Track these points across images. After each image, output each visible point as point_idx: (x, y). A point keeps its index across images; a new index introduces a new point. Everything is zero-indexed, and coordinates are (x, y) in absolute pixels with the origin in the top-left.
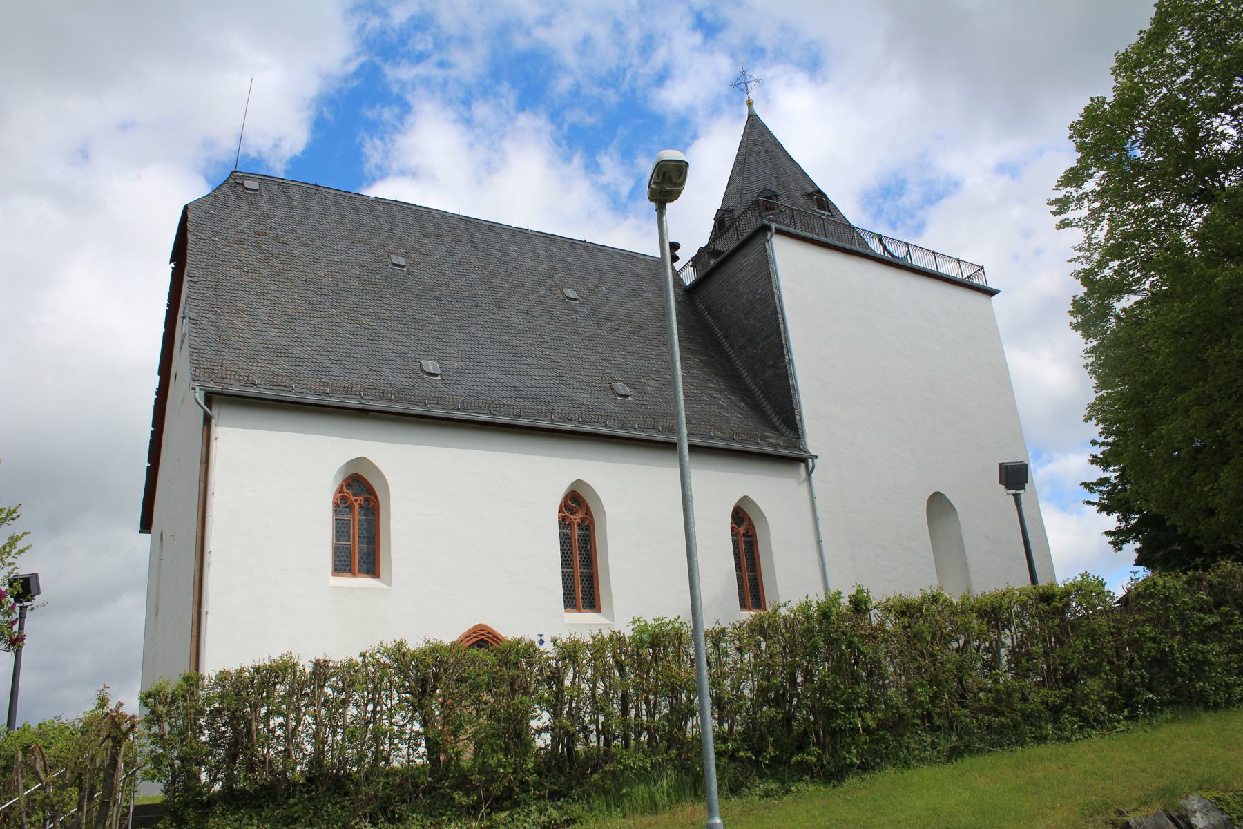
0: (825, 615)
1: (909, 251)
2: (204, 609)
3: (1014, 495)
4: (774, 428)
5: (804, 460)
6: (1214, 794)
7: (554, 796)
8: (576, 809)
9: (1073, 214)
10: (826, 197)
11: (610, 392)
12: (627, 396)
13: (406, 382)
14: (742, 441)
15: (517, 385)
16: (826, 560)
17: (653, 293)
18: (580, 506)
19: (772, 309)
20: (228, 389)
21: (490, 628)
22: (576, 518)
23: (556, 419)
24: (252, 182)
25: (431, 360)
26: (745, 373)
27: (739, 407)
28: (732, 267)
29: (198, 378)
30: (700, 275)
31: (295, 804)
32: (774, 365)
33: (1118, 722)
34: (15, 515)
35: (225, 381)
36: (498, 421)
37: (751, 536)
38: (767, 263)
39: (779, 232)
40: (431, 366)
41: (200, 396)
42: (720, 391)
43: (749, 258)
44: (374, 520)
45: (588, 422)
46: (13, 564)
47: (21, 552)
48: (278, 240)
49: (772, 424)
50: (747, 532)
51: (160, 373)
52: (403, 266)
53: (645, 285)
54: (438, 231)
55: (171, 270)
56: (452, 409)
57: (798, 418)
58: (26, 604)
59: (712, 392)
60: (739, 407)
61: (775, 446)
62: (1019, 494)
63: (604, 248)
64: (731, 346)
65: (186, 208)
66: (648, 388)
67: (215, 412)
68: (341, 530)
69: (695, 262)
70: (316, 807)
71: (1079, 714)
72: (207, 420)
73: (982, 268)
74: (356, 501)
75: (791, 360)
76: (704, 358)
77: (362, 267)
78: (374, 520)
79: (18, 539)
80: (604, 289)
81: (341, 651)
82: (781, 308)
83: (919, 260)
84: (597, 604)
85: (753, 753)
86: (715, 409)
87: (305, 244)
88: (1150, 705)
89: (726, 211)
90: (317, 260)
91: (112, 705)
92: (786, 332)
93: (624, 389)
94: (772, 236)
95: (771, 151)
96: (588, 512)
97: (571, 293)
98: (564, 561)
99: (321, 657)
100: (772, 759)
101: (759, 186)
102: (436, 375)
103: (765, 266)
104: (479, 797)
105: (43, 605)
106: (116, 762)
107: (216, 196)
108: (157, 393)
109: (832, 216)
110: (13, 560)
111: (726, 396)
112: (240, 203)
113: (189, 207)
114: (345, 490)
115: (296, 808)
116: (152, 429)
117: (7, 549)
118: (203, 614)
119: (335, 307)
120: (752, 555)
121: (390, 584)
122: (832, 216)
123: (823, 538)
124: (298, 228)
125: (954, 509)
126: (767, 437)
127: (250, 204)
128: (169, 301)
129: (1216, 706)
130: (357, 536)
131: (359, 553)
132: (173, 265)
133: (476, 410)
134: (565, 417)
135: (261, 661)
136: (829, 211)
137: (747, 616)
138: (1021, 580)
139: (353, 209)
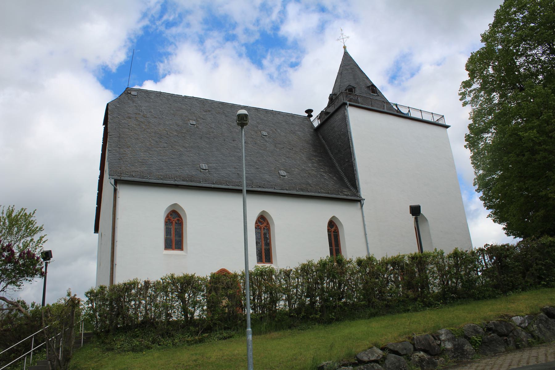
1: (409, 110)
2: (114, 263)
4: (348, 187)
5: (360, 201)
6: (452, 328)
7: (225, 329)
8: (233, 333)
9: (468, 99)
10: (376, 87)
11: (278, 175)
12: (285, 176)
13: (194, 173)
14: (332, 194)
15: (239, 173)
16: (369, 242)
17: (300, 131)
18: (264, 221)
19: (347, 138)
20: (123, 178)
21: (227, 270)
23: (254, 186)
24: (134, 92)
25: (204, 164)
26: (337, 165)
27: (333, 179)
28: (332, 120)
29: (111, 174)
30: (322, 121)
31: (137, 331)
32: (348, 161)
33: (439, 304)
34: (42, 229)
35: (122, 175)
36: (230, 188)
37: (337, 232)
38: (345, 119)
39: (350, 105)
40: (204, 166)
41: (113, 181)
42: (325, 172)
43: (338, 116)
44: (181, 228)
45: (267, 188)
46: (42, 246)
47: (44, 242)
48: (144, 116)
49: (347, 186)
50: (335, 231)
51: (100, 169)
52: (195, 125)
53: (297, 128)
54: (210, 109)
55: (103, 128)
56: (211, 184)
57: (357, 183)
58: (47, 261)
59: (322, 173)
60: (333, 179)
61: (347, 195)
63: (280, 113)
64: (332, 153)
65: (108, 104)
66: (295, 172)
67: (119, 187)
68: (168, 232)
69: (320, 117)
70: (145, 332)
71: (423, 301)
72: (115, 190)
73: (443, 116)
75: (355, 159)
76: (320, 159)
77: (178, 126)
78: (181, 228)
79: (43, 237)
80: (279, 131)
81: (155, 277)
82: (351, 137)
83: (414, 114)
84: (271, 260)
85: (297, 314)
86: (323, 180)
87: (156, 117)
88: (453, 298)
89: (333, 95)
90: (160, 124)
91: (72, 295)
92: (353, 147)
93: (284, 173)
94: (347, 107)
95: (353, 68)
96: (268, 224)
97: (265, 133)
99: (147, 280)
100: (303, 317)
101: (347, 84)
102: (206, 170)
103: (345, 120)
104: (199, 328)
105: (53, 261)
106: (73, 313)
107: (119, 99)
108: (99, 178)
109: (378, 96)
110: (42, 245)
111: (328, 174)
112: (129, 101)
113: (109, 104)
114: (170, 216)
115: (137, 332)
116: (98, 192)
117: (39, 241)
118: (114, 265)
119: (166, 143)
121: (187, 252)
122: (378, 96)
123: (367, 233)
124: (152, 111)
126: (344, 192)
127: (133, 102)
128: (103, 140)
129: (479, 299)
130: (174, 235)
132: (104, 126)
133: (221, 184)
134: (257, 186)
135: (127, 281)
136: (377, 94)
137: (254, 264)
139: (175, 101)
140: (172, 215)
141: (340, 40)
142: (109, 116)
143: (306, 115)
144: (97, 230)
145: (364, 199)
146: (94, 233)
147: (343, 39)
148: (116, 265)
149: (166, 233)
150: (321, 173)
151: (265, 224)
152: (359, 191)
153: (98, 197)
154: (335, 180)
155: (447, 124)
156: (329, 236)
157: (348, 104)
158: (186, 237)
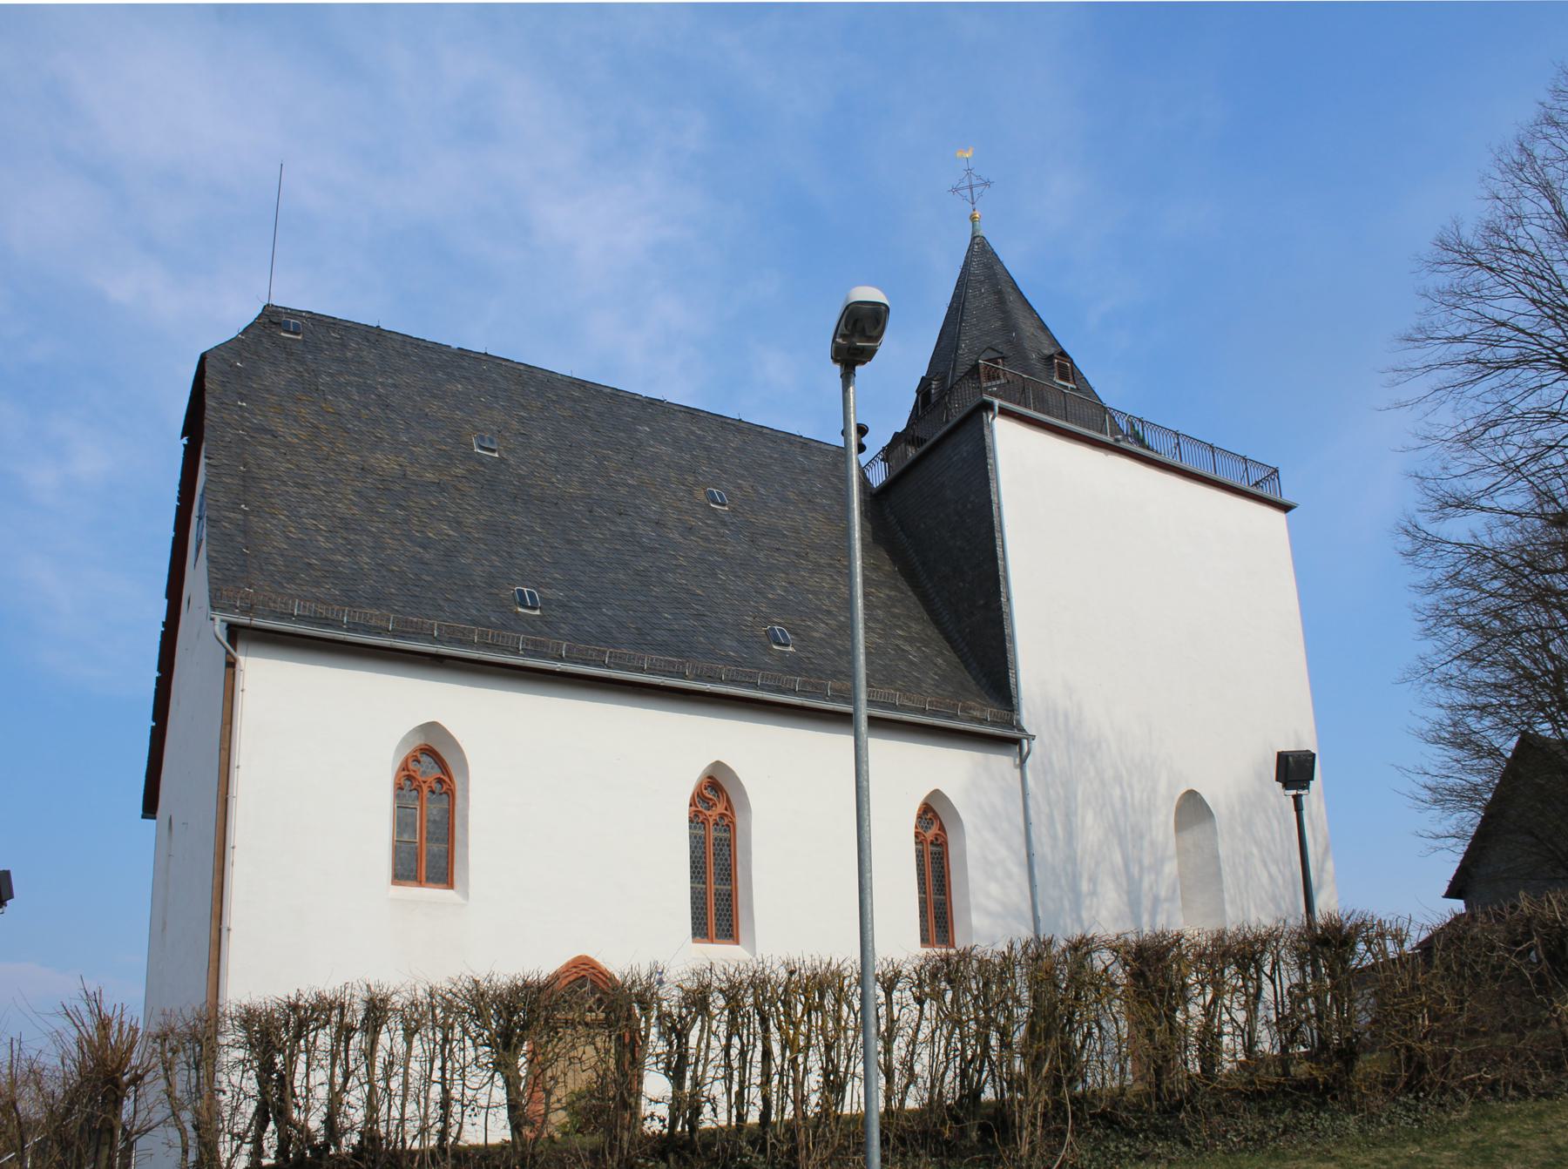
1: (1178, 444)
5: (1016, 742)
22: (713, 814)
38: (984, 458)
39: (1004, 412)
41: (220, 629)
42: (910, 640)
50: (937, 839)
55: (183, 449)
56: (554, 659)
61: (981, 721)
63: (765, 431)
65: (203, 358)
73: (1276, 471)
74: (425, 782)
76: (893, 593)
94: (993, 418)
96: (729, 806)
111: (919, 648)
116: (157, 674)
121: (466, 895)
128: (179, 499)
132: (185, 441)
140: (419, 762)
141: (980, 182)
142: (210, 402)
144: (150, 806)
145: (1034, 737)
146: (143, 817)
147: (971, 187)
148: (229, 930)
150: (898, 642)
151: (720, 808)
152: (1018, 710)
153: (157, 692)
155: (1287, 498)
156: (920, 855)
157: (997, 409)
158: (749, 852)
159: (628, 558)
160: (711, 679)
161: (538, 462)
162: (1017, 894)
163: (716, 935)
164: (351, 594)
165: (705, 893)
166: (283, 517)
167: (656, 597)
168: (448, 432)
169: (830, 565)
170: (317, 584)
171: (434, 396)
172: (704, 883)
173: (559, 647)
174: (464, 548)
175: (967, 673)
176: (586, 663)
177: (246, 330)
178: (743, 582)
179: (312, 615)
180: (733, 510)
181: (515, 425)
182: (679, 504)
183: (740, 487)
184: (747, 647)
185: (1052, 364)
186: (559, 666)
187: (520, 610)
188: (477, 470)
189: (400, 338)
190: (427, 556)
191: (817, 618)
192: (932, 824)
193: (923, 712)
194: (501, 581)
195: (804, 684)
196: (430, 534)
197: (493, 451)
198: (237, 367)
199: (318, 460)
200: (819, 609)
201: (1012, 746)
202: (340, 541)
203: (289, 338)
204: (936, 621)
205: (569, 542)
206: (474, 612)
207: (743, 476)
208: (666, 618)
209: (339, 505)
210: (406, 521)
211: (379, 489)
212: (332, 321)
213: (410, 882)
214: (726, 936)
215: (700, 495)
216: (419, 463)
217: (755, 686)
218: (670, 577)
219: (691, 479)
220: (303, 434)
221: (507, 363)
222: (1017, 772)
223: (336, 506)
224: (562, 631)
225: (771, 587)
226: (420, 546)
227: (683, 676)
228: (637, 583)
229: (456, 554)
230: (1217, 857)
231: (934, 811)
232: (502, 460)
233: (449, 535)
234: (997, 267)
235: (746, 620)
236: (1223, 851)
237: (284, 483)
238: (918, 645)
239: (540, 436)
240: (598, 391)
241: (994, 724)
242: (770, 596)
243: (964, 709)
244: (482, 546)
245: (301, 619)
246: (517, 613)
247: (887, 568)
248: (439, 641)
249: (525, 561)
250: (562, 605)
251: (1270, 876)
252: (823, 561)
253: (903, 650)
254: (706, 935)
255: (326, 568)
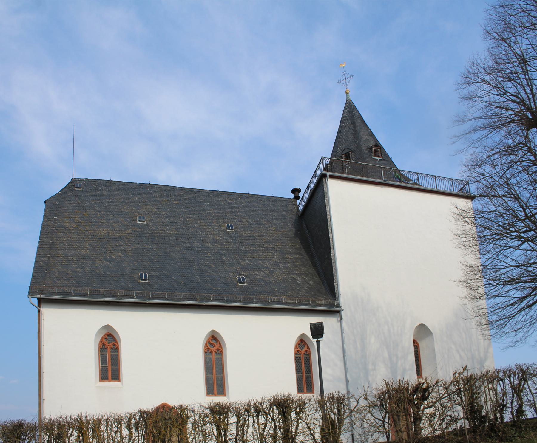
0: (388, 391)
1: (418, 177)
3: (317, 341)
5: (338, 312)
22: (214, 349)
39: (331, 177)
41: (35, 301)
42: (299, 275)
61: (320, 305)
62: (319, 341)
68: (103, 360)
72: (39, 311)
74: (109, 346)
76: (297, 256)
94: (327, 180)
98: (296, 361)
111: (303, 278)
120: (309, 365)
121: (122, 384)
125: (431, 333)
131: (111, 371)
138: (36, 420)
141: (349, 76)
143: (292, 196)
149: (102, 361)
151: (217, 347)
152: (338, 299)
154: (310, 285)
156: (296, 359)
157: (328, 176)
158: (122, 367)
159: (187, 256)
160: (207, 300)
161: (161, 223)
162: (339, 372)
163: (307, 391)
164: (80, 282)
165: (302, 377)
166: (61, 257)
167: (195, 270)
168: (129, 217)
169: (273, 248)
170: (69, 280)
171: (126, 204)
172: (302, 373)
173: (149, 294)
174: (124, 260)
175: (322, 286)
176: (159, 299)
177: (62, 190)
178: (233, 260)
179: (62, 292)
180: (236, 232)
181: (155, 210)
182: (214, 232)
183: (241, 221)
184: (227, 285)
185: (372, 151)
186: (147, 301)
187: (140, 281)
188: (136, 230)
189: (118, 183)
190: (110, 265)
191: (261, 270)
192: (305, 346)
193: (295, 304)
194: (135, 271)
195: (244, 298)
196: (113, 257)
197: (144, 221)
198: (56, 204)
199: (78, 235)
200: (263, 267)
201: (336, 313)
202: (80, 263)
203: (77, 190)
204: (314, 265)
205: (166, 253)
206: (123, 284)
207: (244, 216)
208: (197, 278)
209: (82, 250)
210: (105, 253)
211: (98, 242)
212: (94, 181)
213: (106, 380)
214: (221, 393)
215: (224, 227)
216: (115, 230)
217: (224, 301)
218: (202, 262)
219: (221, 221)
220: (75, 226)
221: (157, 186)
222: (339, 323)
223: (81, 251)
224: (154, 287)
225: (244, 260)
226: (109, 262)
227: (196, 300)
228: (189, 265)
229: (121, 263)
230: (434, 350)
231: (305, 342)
232: (147, 224)
233: (120, 256)
234: (355, 113)
235: (230, 275)
236: (436, 348)
237: (65, 245)
238: (303, 276)
239: (164, 213)
240: (191, 191)
241: (326, 306)
242: (243, 264)
243: (313, 301)
244: (132, 259)
245: (59, 294)
246: (139, 282)
247: (298, 246)
248: (105, 296)
249: (147, 262)
250: (157, 277)
251: (461, 356)
252: (270, 247)
253: (295, 279)
254: (303, 391)
255: (73, 274)
